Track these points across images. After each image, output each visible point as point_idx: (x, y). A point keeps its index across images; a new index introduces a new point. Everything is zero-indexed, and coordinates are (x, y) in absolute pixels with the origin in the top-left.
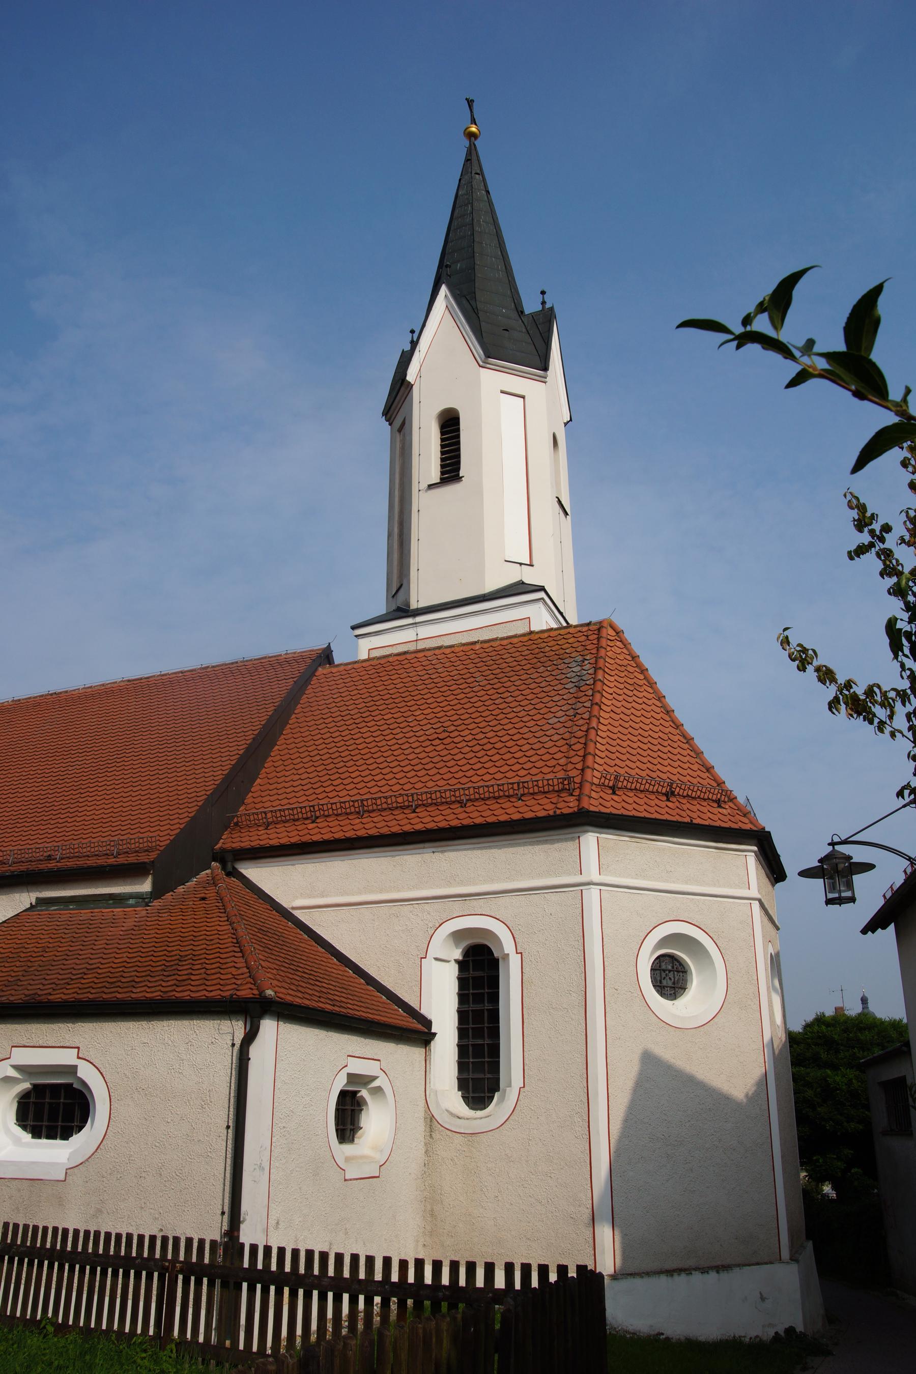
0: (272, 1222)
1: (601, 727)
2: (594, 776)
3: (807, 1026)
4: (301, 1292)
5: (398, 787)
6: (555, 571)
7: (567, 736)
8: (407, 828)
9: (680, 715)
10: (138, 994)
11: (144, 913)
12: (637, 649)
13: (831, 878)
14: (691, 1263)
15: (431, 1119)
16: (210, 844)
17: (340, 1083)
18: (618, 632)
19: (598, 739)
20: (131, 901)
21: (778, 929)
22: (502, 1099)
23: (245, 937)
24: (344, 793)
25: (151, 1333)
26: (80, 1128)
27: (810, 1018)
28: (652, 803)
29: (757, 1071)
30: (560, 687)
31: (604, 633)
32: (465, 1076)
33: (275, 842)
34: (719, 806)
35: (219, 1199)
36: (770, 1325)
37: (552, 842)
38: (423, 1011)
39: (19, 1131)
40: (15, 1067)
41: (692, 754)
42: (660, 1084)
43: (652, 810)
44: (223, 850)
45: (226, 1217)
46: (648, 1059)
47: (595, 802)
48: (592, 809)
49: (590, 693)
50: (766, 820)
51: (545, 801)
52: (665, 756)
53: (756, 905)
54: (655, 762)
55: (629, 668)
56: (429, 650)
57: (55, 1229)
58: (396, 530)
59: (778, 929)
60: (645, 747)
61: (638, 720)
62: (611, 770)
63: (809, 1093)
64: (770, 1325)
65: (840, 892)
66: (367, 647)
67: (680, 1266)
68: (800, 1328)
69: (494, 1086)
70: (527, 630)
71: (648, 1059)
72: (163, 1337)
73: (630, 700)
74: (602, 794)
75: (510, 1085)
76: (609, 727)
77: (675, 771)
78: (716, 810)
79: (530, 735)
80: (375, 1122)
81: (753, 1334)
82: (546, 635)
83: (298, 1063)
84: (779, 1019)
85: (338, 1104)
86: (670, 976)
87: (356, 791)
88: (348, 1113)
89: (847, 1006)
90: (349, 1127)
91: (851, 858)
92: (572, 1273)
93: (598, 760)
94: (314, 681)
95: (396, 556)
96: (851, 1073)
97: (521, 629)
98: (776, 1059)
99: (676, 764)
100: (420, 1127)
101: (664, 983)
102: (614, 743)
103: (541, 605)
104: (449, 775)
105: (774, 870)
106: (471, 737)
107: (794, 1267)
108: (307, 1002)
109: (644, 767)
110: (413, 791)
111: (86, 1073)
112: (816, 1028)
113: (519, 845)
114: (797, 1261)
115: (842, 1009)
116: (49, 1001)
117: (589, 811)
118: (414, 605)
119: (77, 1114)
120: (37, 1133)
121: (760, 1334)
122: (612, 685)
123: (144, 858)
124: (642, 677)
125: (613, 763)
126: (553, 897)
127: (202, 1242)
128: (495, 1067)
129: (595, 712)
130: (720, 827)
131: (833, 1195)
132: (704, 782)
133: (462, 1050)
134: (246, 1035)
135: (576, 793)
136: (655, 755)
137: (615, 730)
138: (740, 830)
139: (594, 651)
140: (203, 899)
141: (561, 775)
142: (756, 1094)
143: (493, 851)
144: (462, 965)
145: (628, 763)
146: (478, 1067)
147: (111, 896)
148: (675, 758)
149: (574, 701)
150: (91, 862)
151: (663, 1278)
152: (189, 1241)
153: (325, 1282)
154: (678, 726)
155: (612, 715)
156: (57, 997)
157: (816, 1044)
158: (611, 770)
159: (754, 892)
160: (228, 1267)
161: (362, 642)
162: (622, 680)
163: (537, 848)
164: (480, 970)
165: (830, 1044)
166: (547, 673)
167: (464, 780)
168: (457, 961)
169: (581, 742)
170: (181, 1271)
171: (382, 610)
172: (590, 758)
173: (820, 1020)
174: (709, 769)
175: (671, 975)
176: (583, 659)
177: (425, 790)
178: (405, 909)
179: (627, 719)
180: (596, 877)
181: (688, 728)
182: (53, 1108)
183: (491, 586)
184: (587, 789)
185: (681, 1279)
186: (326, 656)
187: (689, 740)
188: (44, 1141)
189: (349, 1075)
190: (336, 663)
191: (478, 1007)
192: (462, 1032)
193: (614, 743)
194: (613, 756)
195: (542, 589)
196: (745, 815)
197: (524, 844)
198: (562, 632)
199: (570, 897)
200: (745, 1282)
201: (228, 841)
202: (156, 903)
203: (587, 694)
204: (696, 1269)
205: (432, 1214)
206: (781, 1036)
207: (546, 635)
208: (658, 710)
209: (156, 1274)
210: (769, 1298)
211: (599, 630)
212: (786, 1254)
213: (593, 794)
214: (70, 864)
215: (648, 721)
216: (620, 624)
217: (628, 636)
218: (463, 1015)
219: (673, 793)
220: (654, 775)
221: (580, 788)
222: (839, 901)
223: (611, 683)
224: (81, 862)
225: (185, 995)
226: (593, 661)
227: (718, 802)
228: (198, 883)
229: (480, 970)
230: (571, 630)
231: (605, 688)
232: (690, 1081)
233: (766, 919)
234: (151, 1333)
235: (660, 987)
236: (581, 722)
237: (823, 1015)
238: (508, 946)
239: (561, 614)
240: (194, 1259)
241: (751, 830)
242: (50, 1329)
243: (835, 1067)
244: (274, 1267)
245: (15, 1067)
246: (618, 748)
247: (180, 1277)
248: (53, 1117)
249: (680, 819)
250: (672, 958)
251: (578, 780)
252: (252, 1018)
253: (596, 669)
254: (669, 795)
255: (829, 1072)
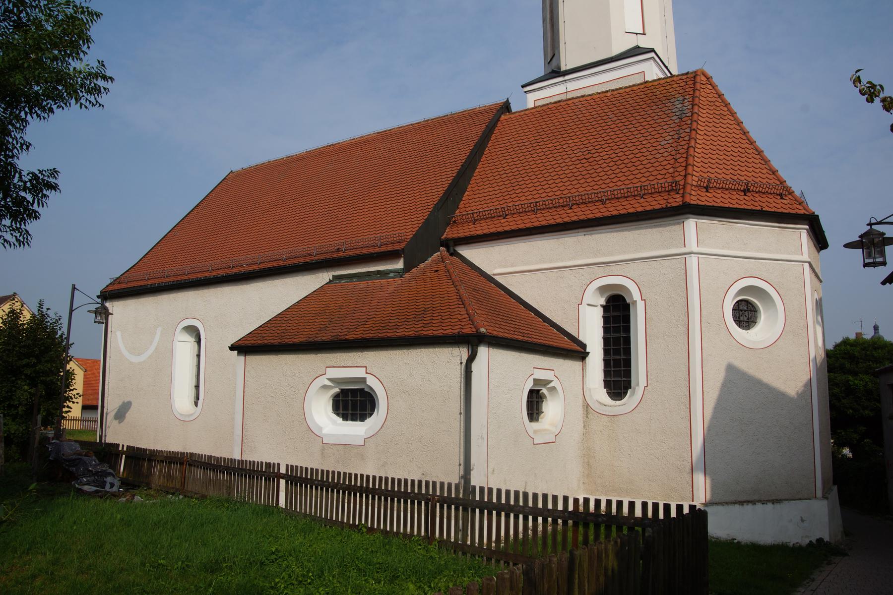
0: (490, 470)
1: (697, 146)
2: (692, 180)
3: (837, 346)
4: (512, 515)
5: (559, 193)
6: (661, 37)
7: (674, 153)
8: (567, 220)
9: (753, 135)
10: (400, 333)
11: (400, 282)
12: (722, 89)
13: (868, 248)
14: (756, 497)
15: (587, 406)
16: (438, 235)
17: (529, 385)
18: (708, 78)
19: (696, 154)
20: (391, 275)
21: (821, 281)
22: (633, 394)
23: (465, 295)
24: (524, 198)
25: (423, 534)
26: (371, 415)
27: (839, 340)
28: (734, 197)
29: (806, 378)
30: (668, 119)
31: (698, 79)
32: (608, 379)
33: (480, 233)
34: (782, 198)
35: (457, 457)
36: (807, 537)
37: (665, 226)
38: (581, 339)
39: (334, 416)
40: (329, 379)
41: (762, 162)
42: (739, 386)
43: (734, 202)
44: (447, 239)
45: (462, 467)
46: (731, 369)
47: (694, 198)
48: (692, 202)
49: (689, 122)
50: (814, 207)
51: (659, 198)
52: (743, 164)
53: (807, 266)
54: (736, 168)
55: (717, 103)
56: (576, 98)
57: (362, 475)
58: (548, 16)
59: (821, 281)
60: (729, 158)
61: (723, 140)
62: (705, 175)
63: (836, 390)
64: (807, 537)
65: (875, 258)
66: (532, 99)
67: (749, 498)
68: (827, 538)
69: (627, 386)
70: (642, 80)
71: (731, 369)
72: (429, 538)
73: (717, 125)
74: (699, 192)
75: (638, 385)
76: (703, 146)
77: (750, 175)
78: (779, 201)
79: (648, 153)
80: (551, 409)
81: (795, 542)
82: (657, 83)
83: (503, 373)
84: (820, 343)
85: (528, 398)
86: (745, 314)
87: (531, 197)
88: (535, 402)
89: (864, 332)
90: (535, 411)
91: (884, 234)
92: (686, 510)
93: (695, 168)
94: (499, 124)
95: (549, 34)
96: (866, 378)
97: (639, 80)
98: (818, 370)
99: (750, 170)
100: (580, 411)
101: (742, 318)
102: (707, 156)
103: (652, 62)
104: (593, 183)
105: (820, 241)
106: (607, 157)
107: (825, 502)
108: (507, 335)
109: (728, 172)
110: (569, 195)
111: (372, 382)
112: (843, 347)
113: (641, 228)
114: (827, 498)
115: (861, 334)
116: (346, 340)
117: (690, 204)
118: (563, 68)
119: (368, 406)
120: (345, 418)
121: (799, 541)
122: (704, 116)
123: (397, 247)
124: (726, 109)
125: (706, 170)
126: (666, 262)
127: (450, 485)
128: (628, 374)
129: (693, 136)
130: (782, 213)
131: (850, 455)
132: (771, 182)
133: (607, 363)
134: (469, 357)
135: (681, 192)
136: (735, 164)
137: (708, 148)
138: (797, 214)
139: (691, 93)
140: (437, 271)
141: (670, 180)
142: (804, 392)
143: (625, 233)
144: (605, 308)
145: (717, 170)
146: (617, 374)
147: (378, 272)
148: (750, 165)
149: (677, 128)
150: (365, 251)
151: (737, 506)
152: (442, 484)
153: (527, 510)
154: (752, 143)
155: (705, 137)
156: (350, 337)
157: (843, 358)
158: (705, 175)
159: (806, 257)
160: (467, 500)
161: (529, 95)
162: (711, 112)
163: (655, 230)
164: (617, 311)
165: (852, 358)
166: (658, 110)
167: (604, 186)
168: (602, 306)
169: (683, 157)
170: (438, 501)
171: (541, 73)
172: (690, 168)
173: (846, 342)
174: (774, 172)
175: (746, 313)
176: (682, 99)
177: (577, 193)
178: (567, 273)
179: (716, 139)
180: (695, 249)
181: (760, 144)
182: (354, 403)
183: (616, 51)
184: (688, 187)
185: (749, 507)
186: (506, 107)
187: (760, 152)
188: (350, 422)
189: (535, 380)
190: (513, 111)
191: (617, 335)
192: (606, 352)
193: (707, 156)
194: (706, 166)
195: (653, 50)
196: (800, 204)
197: (646, 228)
198: (668, 80)
199: (677, 262)
200: (791, 511)
201: (449, 233)
202: (407, 275)
203: (687, 123)
204: (758, 501)
205: (588, 464)
206: (822, 354)
207: (657, 83)
208: (738, 132)
209: (423, 503)
210: (806, 520)
211: (695, 77)
212: (819, 493)
213: (693, 193)
214: (351, 253)
215: (730, 140)
216: (710, 73)
217: (715, 80)
218: (606, 341)
219: (748, 190)
220: (735, 178)
221: (684, 188)
222: (874, 265)
223: (703, 114)
224: (358, 252)
225: (429, 333)
226: (691, 99)
227: (781, 195)
228: (432, 261)
229: (617, 311)
230: (674, 79)
231: (700, 118)
232: (759, 383)
233: (813, 275)
234: (423, 534)
235: (739, 322)
236: (683, 143)
237: (848, 339)
238: (636, 296)
239: (666, 67)
240: (446, 495)
241: (804, 214)
242: (365, 530)
243: (855, 374)
244: (495, 500)
245: (329, 379)
246: (710, 160)
247: (438, 505)
248: (354, 408)
249: (754, 208)
250: (747, 302)
251: (682, 183)
252: (472, 346)
253: (693, 105)
254: (746, 191)
255: (851, 378)
